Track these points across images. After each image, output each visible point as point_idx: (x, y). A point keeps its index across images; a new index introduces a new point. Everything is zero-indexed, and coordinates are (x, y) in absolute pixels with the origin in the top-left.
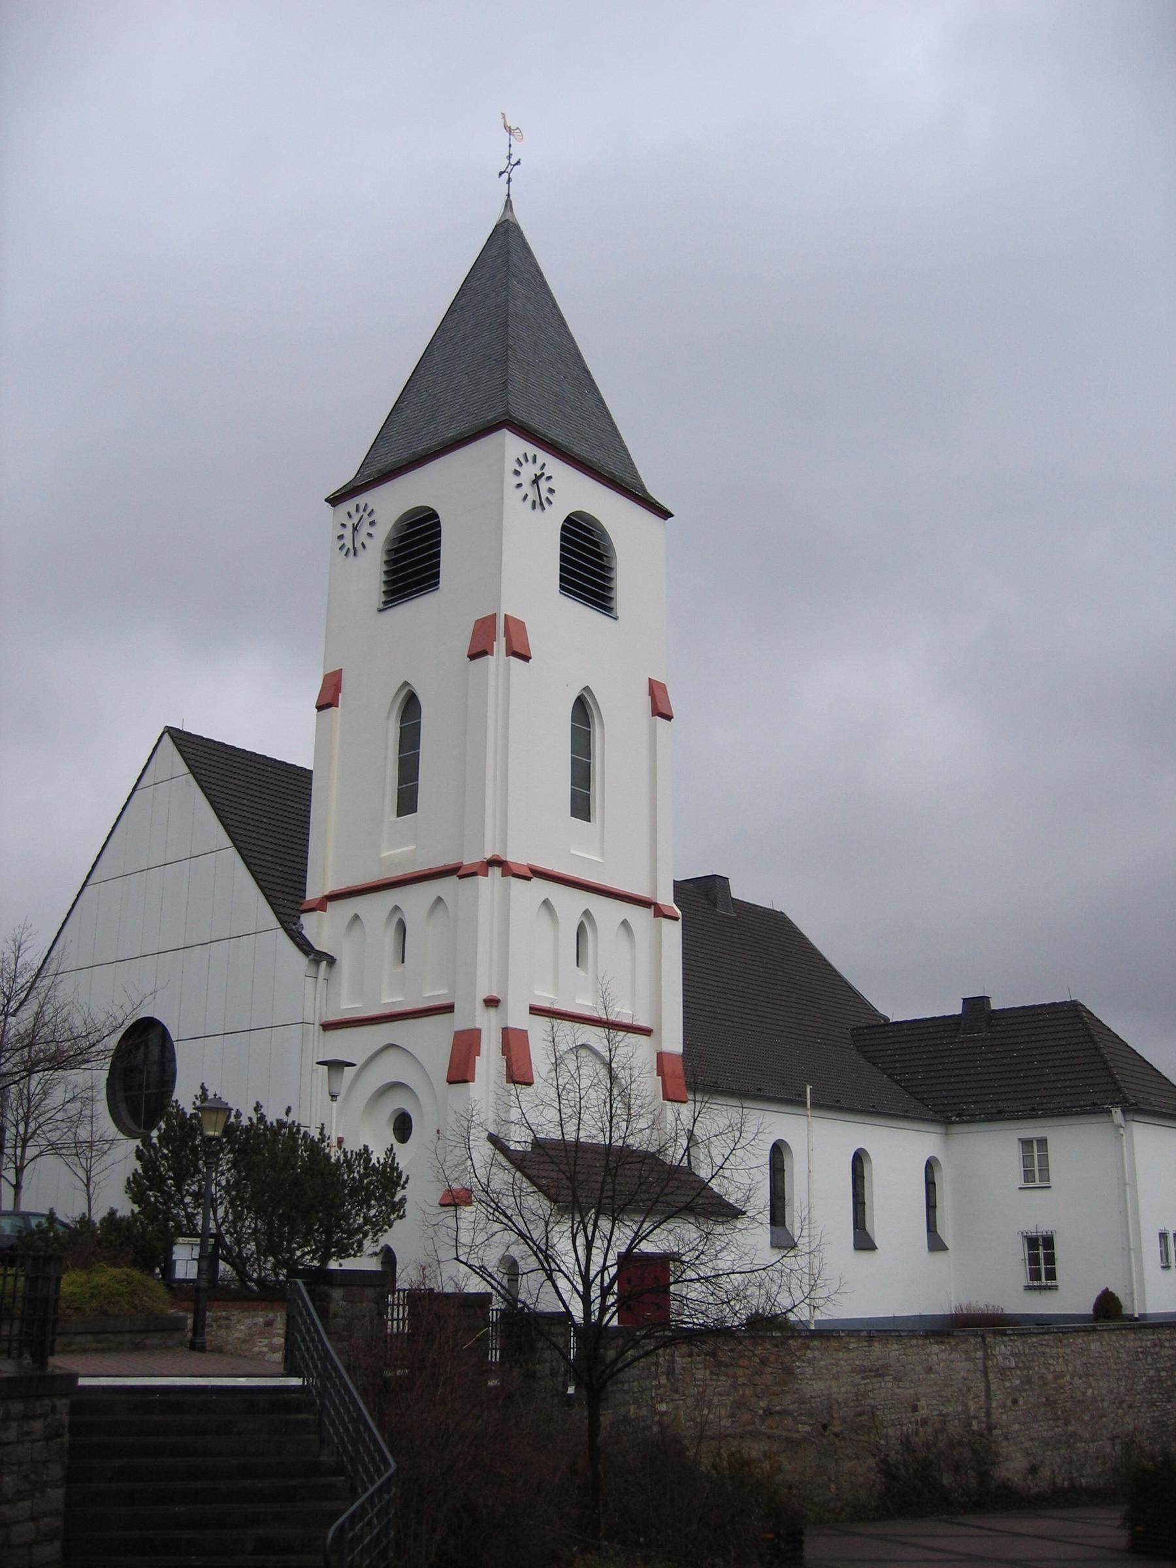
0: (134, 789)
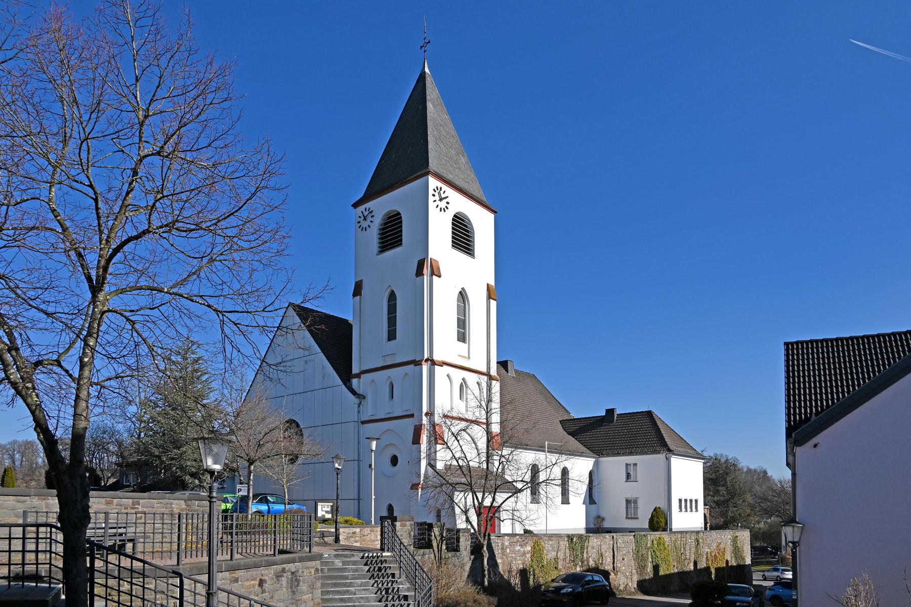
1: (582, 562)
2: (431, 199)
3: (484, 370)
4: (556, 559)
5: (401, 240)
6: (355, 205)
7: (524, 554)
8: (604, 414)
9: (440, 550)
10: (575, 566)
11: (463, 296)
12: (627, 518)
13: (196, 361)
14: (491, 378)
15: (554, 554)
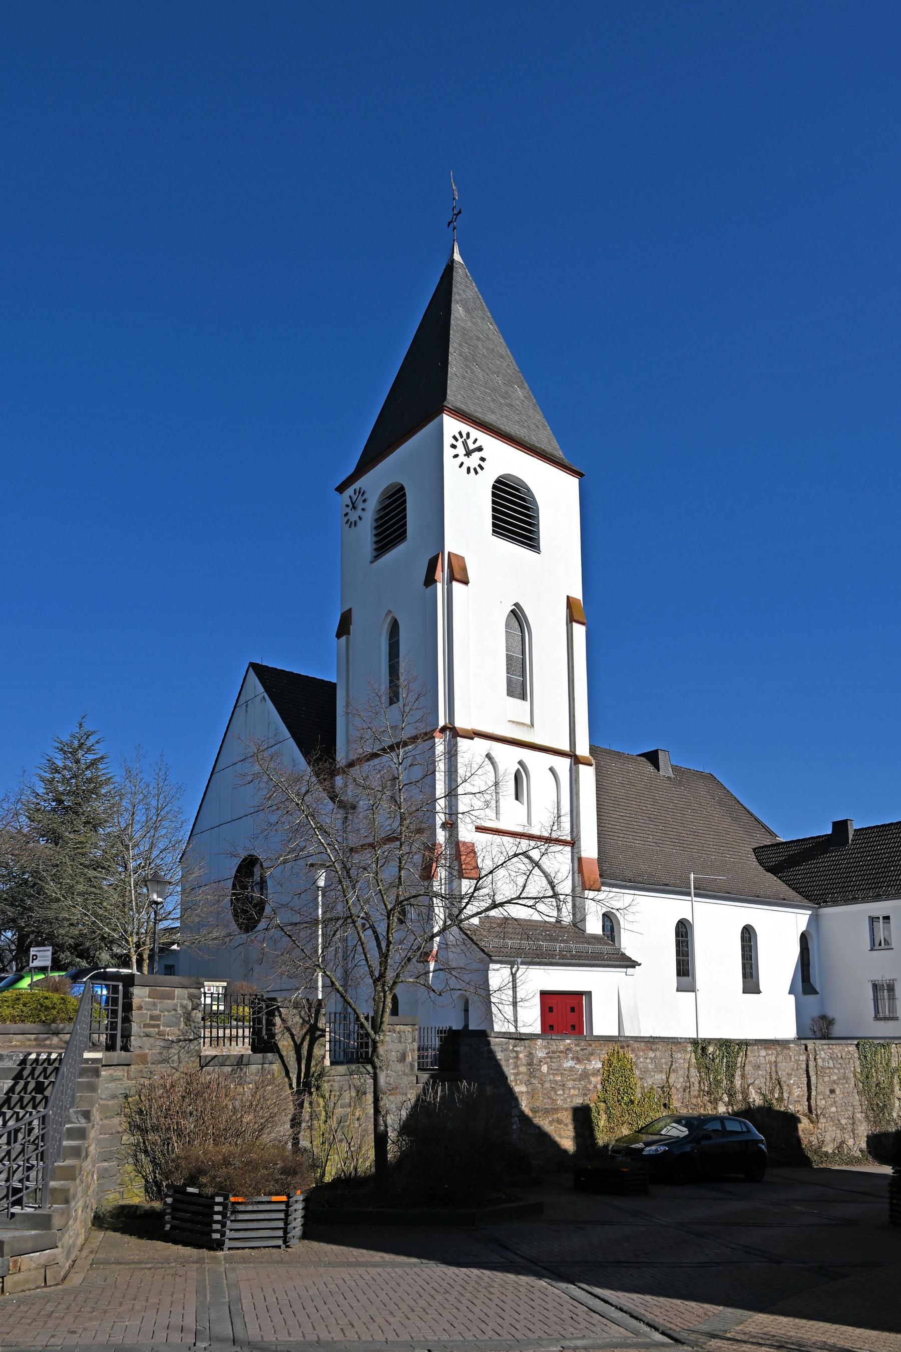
0: (235, 707)
1: (731, 1096)
2: (448, 452)
3: (566, 747)
4: (666, 1088)
5: (405, 532)
6: (341, 489)
7: (585, 1075)
8: (829, 831)
9: (305, 1057)
10: (715, 1102)
12: (877, 1018)
13: (93, 763)
15: (660, 1077)
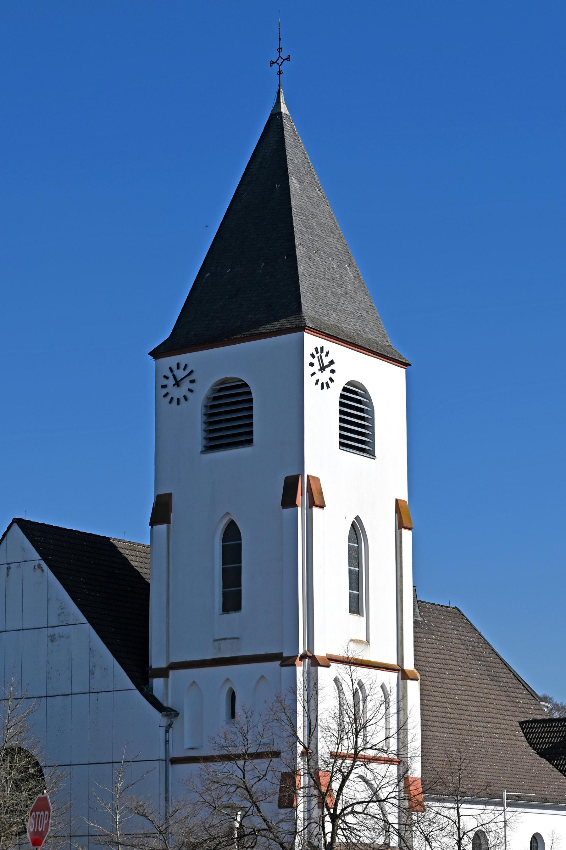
2: (308, 370)
3: (392, 661)
6: (156, 354)
11: (357, 531)
14: (404, 676)
